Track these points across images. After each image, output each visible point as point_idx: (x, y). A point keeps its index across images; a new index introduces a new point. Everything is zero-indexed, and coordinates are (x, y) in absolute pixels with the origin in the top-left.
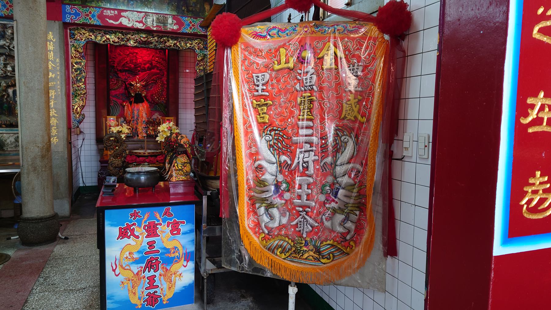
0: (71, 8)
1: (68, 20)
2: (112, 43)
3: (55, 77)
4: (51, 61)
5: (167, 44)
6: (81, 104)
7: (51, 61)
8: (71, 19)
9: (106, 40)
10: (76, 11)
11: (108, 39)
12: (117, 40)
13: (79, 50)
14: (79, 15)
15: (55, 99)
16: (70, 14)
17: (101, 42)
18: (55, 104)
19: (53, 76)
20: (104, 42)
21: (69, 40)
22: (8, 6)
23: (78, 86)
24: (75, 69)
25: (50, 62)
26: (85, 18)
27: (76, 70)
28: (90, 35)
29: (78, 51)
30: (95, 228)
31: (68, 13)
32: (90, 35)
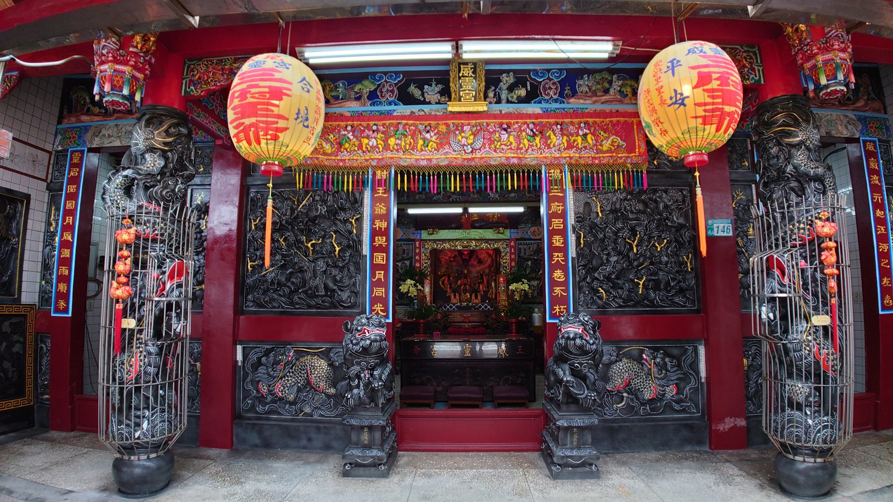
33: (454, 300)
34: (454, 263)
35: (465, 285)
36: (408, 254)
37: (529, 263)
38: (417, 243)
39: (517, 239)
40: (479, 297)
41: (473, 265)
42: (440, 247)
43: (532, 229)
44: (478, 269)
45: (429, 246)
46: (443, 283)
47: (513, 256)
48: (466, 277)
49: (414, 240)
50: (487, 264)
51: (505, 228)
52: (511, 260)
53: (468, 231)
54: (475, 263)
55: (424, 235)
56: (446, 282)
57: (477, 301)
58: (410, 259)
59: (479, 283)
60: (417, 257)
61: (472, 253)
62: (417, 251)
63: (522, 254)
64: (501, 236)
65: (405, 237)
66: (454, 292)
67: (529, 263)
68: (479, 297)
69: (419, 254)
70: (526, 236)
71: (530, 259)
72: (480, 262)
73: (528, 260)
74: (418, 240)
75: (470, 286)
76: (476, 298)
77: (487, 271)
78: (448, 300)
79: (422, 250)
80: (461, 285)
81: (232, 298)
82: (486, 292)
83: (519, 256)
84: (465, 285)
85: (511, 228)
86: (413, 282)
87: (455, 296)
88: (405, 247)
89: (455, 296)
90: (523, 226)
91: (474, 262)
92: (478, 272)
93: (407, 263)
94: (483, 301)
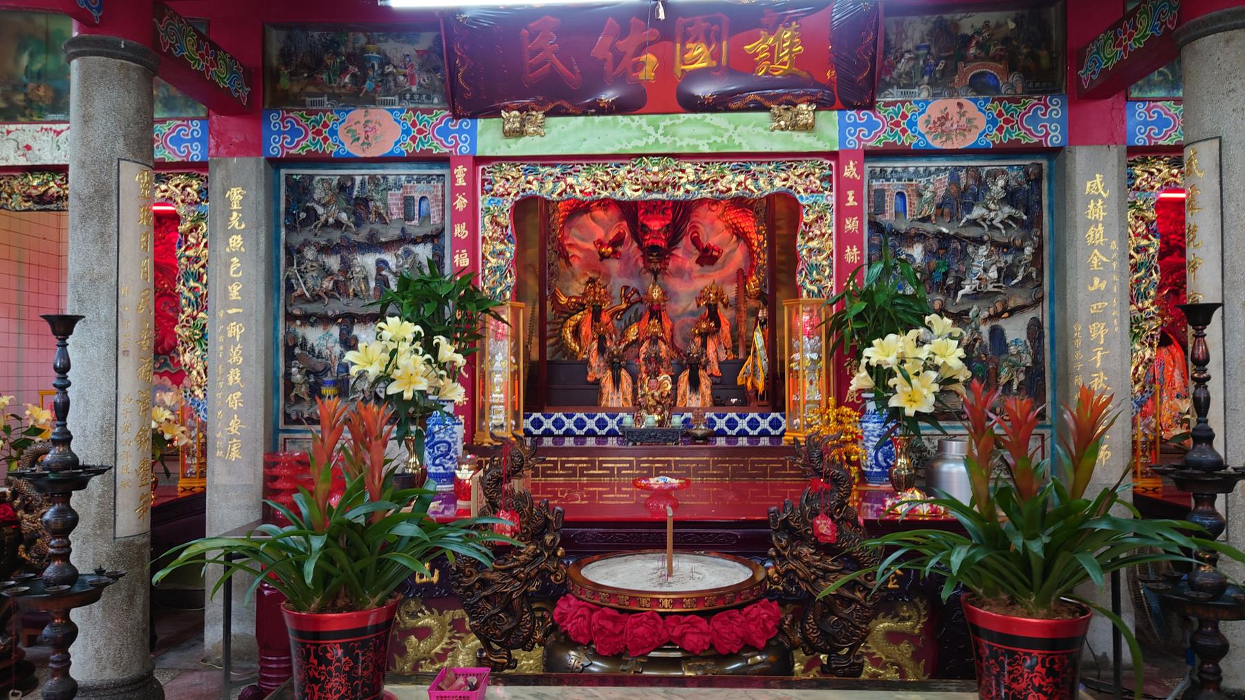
0: (1148, 110)
1: (1140, 140)
2: (579, 195)
3: (1108, 289)
4: (1099, 248)
5: (721, 186)
6: (1147, 356)
7: (1099, 248)
8: (1149, 137)
9: (565, 190)
10: (1160, 114)
11: (571, 186)
12: (590, 187)
13: (501, 220)
14: (1167, 123)
15: (1106, 347)
16: (279, 133)
17: (554, 196)
18: (1104, 358)
19: (1103, 286)
20: (560, 194)
21: (481, 198)
22: (414, 132)
23: (1141, 310)
24: (490, 269)
25: (1096, 251)
26: (892, 130)
27: (493, 271)
28: (529, 182)
29: (498, 224)
30: (233, 632)
31: (275, 133)
32: (529, 182)
33: (613, 398)
34: (614, 265)
35: (654, 340)
36: (425, 217)
37: (917, 251)
38: (460, 172)
39: (872, 154)
40: (705, 383)
41: (680, 273)
42: (548, 186)
43: (936, 108)
44: (700, 284)
45: (513, 184)
46: (576, 333)
47: (851, 224)
48: (656, 312)
49: (444, 160)
50: (731, 270)
51: (823, 105)
52: (844, 239)
53: (665, 120)
54: (691, 263)
55: (489, 137)
56: (585, 329)
57: (695, 401)
58: (434, 238)
59: (704, 336)
60: (461, 231)
61: (682, 212)
62: (461, 203)
63: (888, 218)
64: (801, 142)
65: (408, 148)
66: (615, 365)
67: (917, 251)
68: (705, 383)
69: (471, 217)
70: (909, 140)
71: (921, 237)
72: (708, 257)
73: (909, 238)
74: (462, 159)
75: (672, 346)
76: (695, 384)
77: (730, 292)
78: (590, 397)
79: (483, 201)
80: (637, 343)
81: (537, 348)
82: (732, 367)
83: (875, 227)
84: (654, 340)
85: (847, 106)
86: (411, 329)
87: (617, 381)
88: (417, 191)
89: (617, 381)
90: (894, 95)
91: (685, 255)
92: (702, 296)
93: (424, 252)
94: (719, 402)
